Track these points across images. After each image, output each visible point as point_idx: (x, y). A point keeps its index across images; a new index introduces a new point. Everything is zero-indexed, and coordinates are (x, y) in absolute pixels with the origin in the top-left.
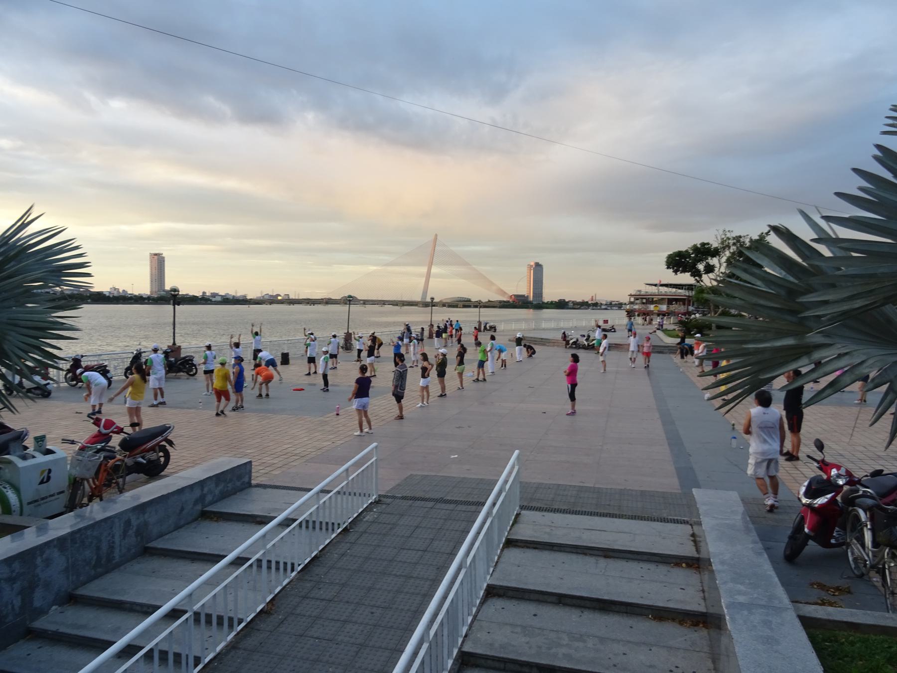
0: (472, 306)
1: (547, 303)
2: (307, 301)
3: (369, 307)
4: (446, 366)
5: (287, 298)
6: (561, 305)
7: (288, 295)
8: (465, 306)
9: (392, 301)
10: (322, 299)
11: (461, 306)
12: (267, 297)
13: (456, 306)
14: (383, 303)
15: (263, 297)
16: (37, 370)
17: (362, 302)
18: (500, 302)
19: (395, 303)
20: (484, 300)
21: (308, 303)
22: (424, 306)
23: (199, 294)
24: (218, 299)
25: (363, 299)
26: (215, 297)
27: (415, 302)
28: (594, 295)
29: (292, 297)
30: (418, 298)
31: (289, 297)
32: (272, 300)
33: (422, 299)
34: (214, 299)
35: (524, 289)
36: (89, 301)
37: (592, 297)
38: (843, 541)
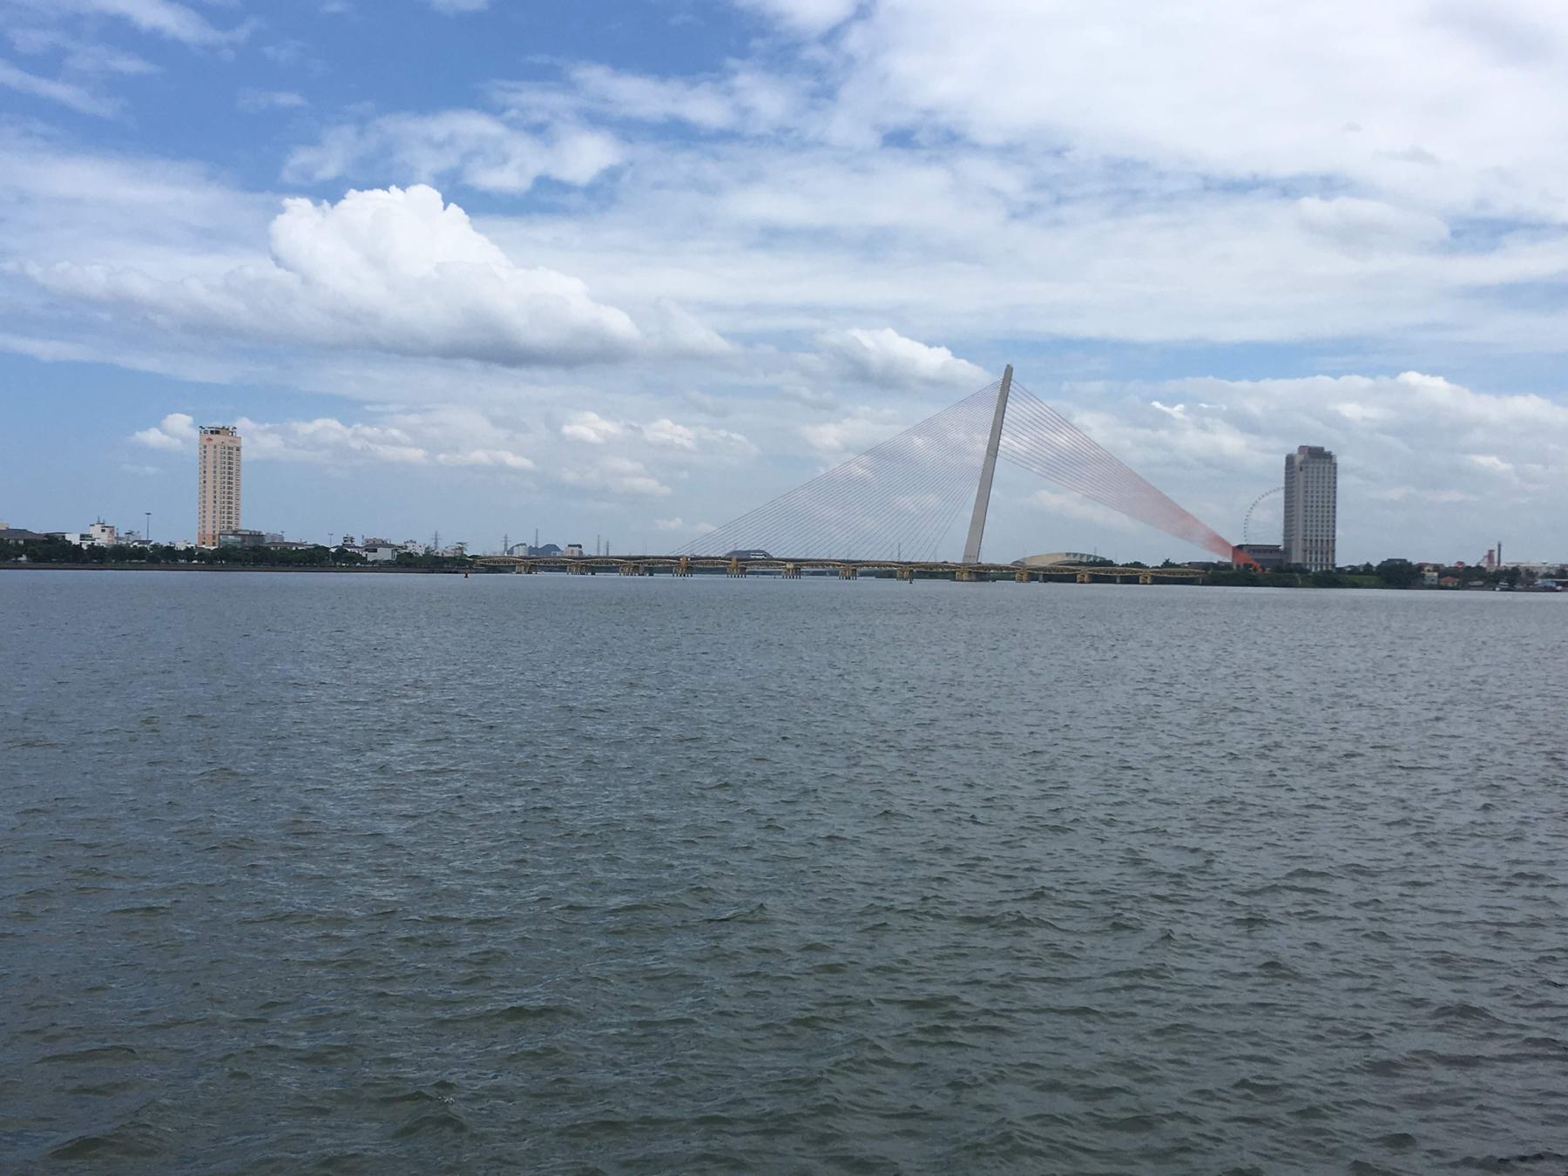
0: (1118, 580)
1: (1354, 570)
2: (632, 563)
3: (807, 583)
4: (317, 547)
5: (576, 554)
6: (1398, 575)
7: (580, 546)
8: (1095, 579)
9: (879, 564)
10: (678, 558)
11: (1086, 579)
12: (520, 552)
13: (1071, 579)
14: (852, 569)
15: (511, 552)
16: (1202, 408)
17: (790, 566)
18: (1206, 566)
19: (885, 571)
20: (1153, 560)
21: (636, 569)
22: (973, 577)
23: (332, 543)
24: (384, 555)
25: (792, 557)
26: (375, 551)
27: (944, 565)
28: (1495, 548)
29: (589, 551)
30: (954, 554)
31: (581, 552)
32: (542, 561)
33: (965, 556)
34: (371, 557)
35: (1267, 528)
36: (24, 558)
37: (1491, 552)
38: (1145, 1143)
